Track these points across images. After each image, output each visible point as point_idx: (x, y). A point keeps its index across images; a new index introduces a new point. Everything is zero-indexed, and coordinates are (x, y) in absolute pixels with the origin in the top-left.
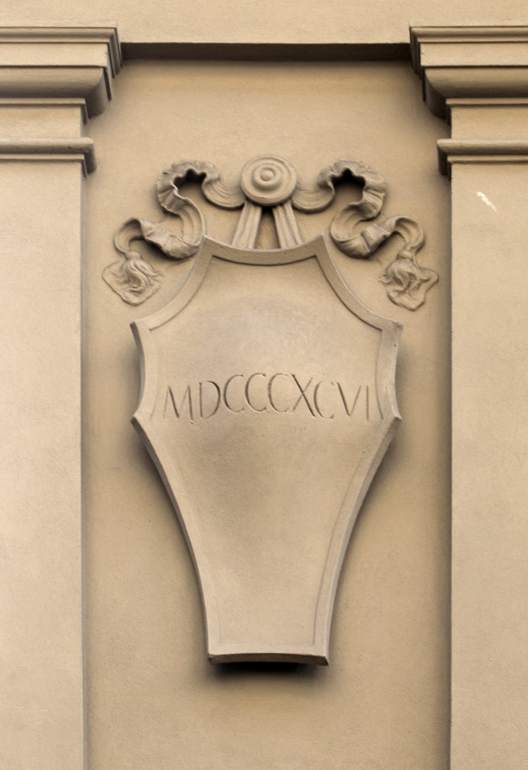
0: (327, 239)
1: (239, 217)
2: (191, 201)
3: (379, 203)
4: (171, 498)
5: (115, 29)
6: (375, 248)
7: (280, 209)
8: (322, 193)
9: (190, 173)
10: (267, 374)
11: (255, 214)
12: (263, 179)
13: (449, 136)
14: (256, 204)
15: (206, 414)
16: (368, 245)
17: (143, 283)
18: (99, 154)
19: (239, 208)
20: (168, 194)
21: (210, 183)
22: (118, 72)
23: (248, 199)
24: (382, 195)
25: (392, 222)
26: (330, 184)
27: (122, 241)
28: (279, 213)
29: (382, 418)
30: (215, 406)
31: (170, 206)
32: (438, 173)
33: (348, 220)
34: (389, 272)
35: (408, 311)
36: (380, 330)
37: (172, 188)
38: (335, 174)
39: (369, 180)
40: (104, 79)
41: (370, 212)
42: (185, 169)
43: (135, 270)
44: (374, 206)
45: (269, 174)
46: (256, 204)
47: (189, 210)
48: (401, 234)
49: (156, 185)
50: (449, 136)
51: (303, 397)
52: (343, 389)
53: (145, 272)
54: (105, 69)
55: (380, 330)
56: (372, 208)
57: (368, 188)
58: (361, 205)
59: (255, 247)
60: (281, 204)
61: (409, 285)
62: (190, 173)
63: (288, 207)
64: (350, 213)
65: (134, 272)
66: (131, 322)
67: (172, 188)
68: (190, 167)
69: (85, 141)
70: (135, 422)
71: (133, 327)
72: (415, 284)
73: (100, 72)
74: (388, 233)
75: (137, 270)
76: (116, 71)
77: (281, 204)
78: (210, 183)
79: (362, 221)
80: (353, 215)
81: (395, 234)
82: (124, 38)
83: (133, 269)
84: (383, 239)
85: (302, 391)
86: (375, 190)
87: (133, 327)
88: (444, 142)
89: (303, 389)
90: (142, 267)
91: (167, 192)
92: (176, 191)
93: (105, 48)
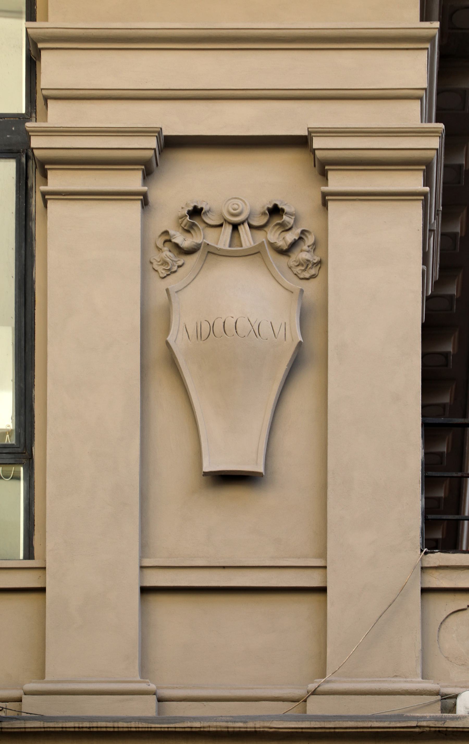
0: (265, 242)
1: (221, 231)
2: (196, 222)
3: (292, 221)
4: (182, 376)
5: (161, 129)
6: (290, 246)
7: (242, 226)
8: (263, 217)
9: (195, 207)
10: (234, 317)
11: (228, 229)
12: (235, 210)
13: (327, 185)
14: (230, 223)
15: (203, 339)
16: (286, 244)
17: (170, 264)
18: (151, 198)
19: (221, 225)
20: (184, 220)
21: (205, 213)
22: (162, 151)
23: (225, 220)
24: (293, 217)
25: (299, 231)
26: (267, 212)
27: (160, 243)
28: (241, 228)
29: (293, 340)
30: (208, 334)
31: (185, 226)
32: (321, 205)
33: (275, 232)
34: (297, 259)
35: (299, 279)
36: (292, 292)
37: (186, 216)
38: (268, 206)
39: (286, 209)
40: (154, 155)
41: (287, 226)
42: (193, 205)
43: (167, 258)
44: (289, 223)
45: (236, 206)
46: (230, 223)
47: (195, 228)
48: (303, 238)
49: (178, 214)
50: (327, 185)
51: (252, 329)
52: (273, 324)
53: (171, 259)
54: (155, 149)
55: (292, 292)
56: (288, 224)
57: (286, 213)
58: (283, 222)
59: (230, 246)
60: (242, 223)
61: (307, 266)
62: (195, 207)
63: (246, 225)
64: (277, 227)
65: (166, 259)
66: (166, 288)
67: (186, 216)
68: (196, 204)
69: (145, 189)
70: (167, 343)
71: (167, 290)
72: (310, 266)
73: (153, 151)
74: (297, 238)
75: (168, 258)
76: (161, 151)
77: (242, 223)
78: (205, 213)
79: (283, 231)
80: (279, 228)
81: (300, 238)
82: (166, 132)
83: (166, 258)
84: (294, 241)
85: (252, 327)
86: (290, 215)
87: (167, 290)
88: (324, 189)
89: (253, 326)
90: (170, 256)
91: (184, 218)
92: (188, 218)
93: (155, 139)
